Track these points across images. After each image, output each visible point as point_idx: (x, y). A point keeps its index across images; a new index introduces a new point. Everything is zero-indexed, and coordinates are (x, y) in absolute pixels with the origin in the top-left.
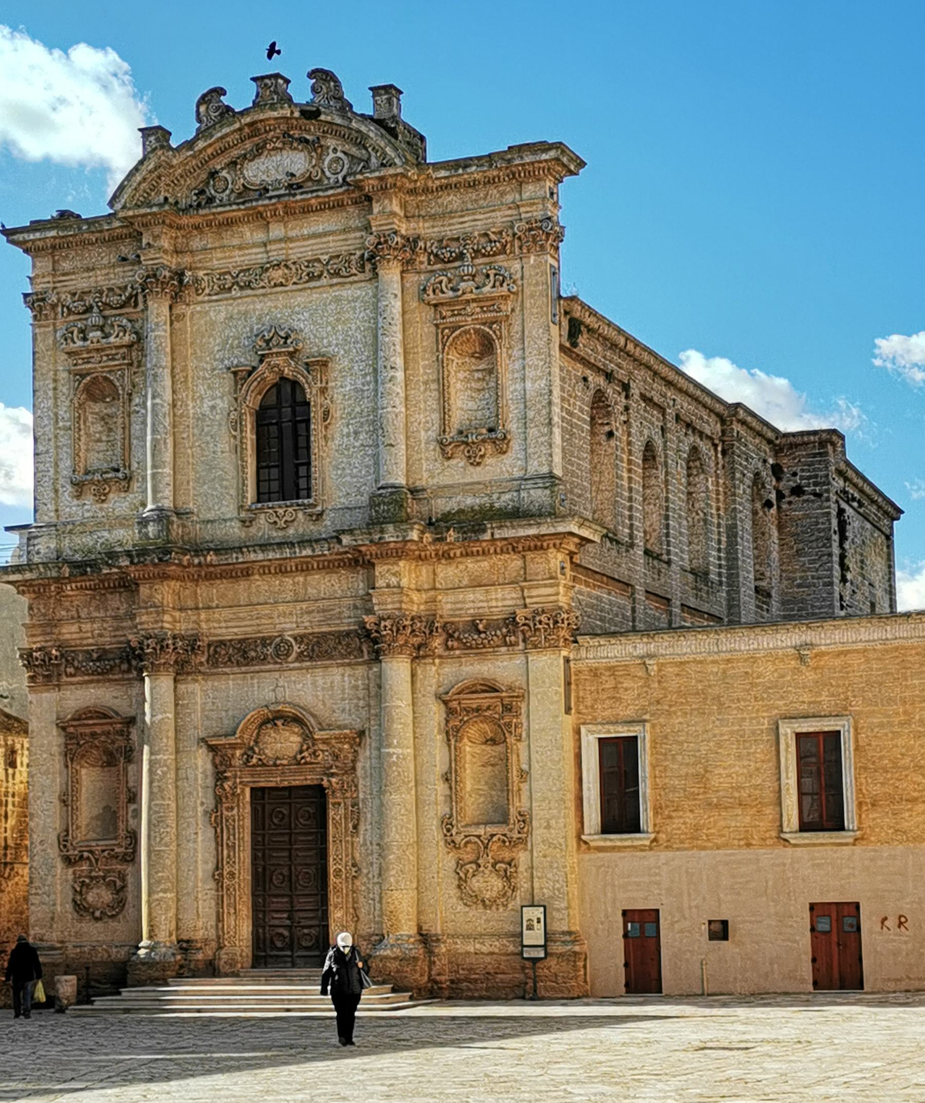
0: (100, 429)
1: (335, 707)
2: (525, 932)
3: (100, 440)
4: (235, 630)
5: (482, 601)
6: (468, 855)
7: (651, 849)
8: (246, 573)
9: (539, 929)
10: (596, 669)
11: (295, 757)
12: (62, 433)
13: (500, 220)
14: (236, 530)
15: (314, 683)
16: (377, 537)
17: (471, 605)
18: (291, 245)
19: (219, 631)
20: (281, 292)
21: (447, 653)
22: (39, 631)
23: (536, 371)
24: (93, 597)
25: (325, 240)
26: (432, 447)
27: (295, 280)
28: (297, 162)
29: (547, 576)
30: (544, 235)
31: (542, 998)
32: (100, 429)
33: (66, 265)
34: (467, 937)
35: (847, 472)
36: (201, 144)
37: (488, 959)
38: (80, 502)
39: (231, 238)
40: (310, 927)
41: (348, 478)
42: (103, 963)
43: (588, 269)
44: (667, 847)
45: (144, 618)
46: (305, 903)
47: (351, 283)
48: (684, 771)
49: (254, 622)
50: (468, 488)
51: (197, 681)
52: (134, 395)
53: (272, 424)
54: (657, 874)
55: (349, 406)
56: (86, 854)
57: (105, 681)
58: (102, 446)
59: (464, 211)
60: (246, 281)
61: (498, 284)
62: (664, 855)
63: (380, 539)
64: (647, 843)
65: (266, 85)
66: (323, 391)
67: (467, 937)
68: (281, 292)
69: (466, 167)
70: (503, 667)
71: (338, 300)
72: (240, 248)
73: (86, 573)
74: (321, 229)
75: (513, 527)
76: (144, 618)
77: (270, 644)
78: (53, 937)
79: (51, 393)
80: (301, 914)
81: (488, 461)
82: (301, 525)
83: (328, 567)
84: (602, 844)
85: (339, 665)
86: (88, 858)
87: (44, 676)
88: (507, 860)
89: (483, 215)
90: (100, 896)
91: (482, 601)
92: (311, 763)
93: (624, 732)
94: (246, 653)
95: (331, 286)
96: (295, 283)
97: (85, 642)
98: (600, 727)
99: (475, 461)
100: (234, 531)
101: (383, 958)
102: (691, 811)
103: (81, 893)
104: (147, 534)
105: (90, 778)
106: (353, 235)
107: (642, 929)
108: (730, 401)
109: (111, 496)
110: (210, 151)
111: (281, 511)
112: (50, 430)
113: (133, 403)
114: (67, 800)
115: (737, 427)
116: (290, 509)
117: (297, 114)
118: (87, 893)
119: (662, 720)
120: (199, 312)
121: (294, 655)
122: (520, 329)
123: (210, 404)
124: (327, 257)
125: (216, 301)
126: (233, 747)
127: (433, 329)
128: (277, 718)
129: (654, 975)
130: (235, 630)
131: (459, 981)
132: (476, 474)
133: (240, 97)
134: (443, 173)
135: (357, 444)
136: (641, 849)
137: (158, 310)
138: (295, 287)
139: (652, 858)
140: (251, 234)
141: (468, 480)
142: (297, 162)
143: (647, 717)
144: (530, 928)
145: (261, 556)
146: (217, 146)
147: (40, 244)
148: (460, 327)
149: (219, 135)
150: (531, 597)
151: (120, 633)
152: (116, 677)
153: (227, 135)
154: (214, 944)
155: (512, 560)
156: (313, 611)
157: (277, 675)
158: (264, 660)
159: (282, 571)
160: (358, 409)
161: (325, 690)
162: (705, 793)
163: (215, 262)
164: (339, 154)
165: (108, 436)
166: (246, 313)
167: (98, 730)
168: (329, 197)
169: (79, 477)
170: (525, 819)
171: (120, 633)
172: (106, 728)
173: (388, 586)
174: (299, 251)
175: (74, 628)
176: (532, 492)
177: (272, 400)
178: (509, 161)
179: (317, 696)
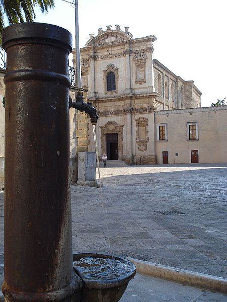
23: (151, 73)
30: (151, 50)
35: (195, 88)
43: (156, 55)
60: (106, 57)
66: (117, 74)
70: (146, 116)
82: (114, 94)
89: (144, 47)
100: (104, 95)
107: (165, 154)
108: (186, 80)
112: (8, 181)
115: (179, 80)
128: (111, 123)
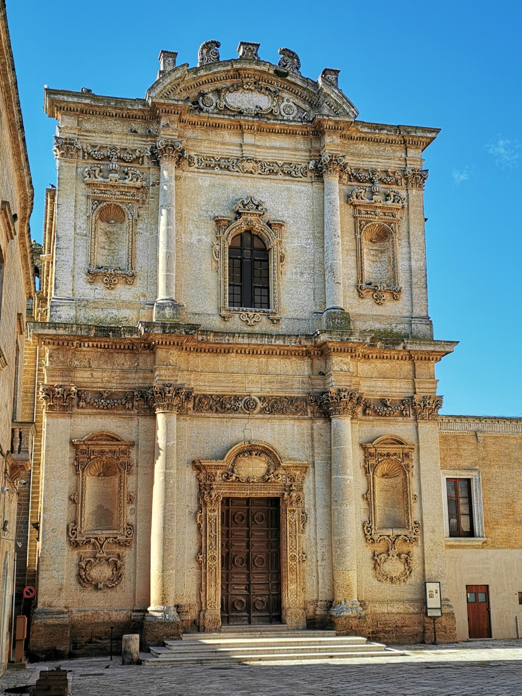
0: (104, 240)
1: (287, 446)
2: (428, 598)
3: (103, 248)
4: (216, 388)
5: (386, 388)
6: (380, 548)
7: (483, 548)
8: (227, 351)
9: (437, 596)
10: (446, 436)
11: (263, 477)
12: (79, 237)
13: (393, 165)
14: (217, 323)
15: (273, 429)
16: (346, 338)
17: (379, 389)
18: (258, 150)
19: (203, 388)
20: (250, 177)
21: (364, 418)
22: (58, 373)
24: (102, 353)
25: (281, 152)
26: (352, 290)
27: (260, 172)
28: (264, 102)
29: (429, 377)
31: (441, 643)
32: (104, 240)
33: (87, 126)
34: (382, 602)
36: (202, 73)
37: (397, 617)
38: (93, 286)
39: (214, 135)
40: (262, 595)
41: (296, 301)
42: (104, 623)
44: (492, 546)
45: (162, 372)
46: (259, 578)
47: (298, 181)
48: (500, 500)
49: (230, 385)
50: (377, 318)
51: (186, 420)
52: (139, 222)
53: (237, 259)
54: (487, 563)
55: (297, 256)
56: (93, 540)
57: (111, 414)
58: (105, 252)
59: (371, 156)
60: (225, 165)
61: (396, 201)
62: (491, 552)
63: (348, 339)
64: (480, 543)
65: (250, 49)
67: (382, 602)
68: (250, 177)
69: (382, 129)
71: (288, 189)
72: (223, 144)
73: (108, 336)
74: (278, 144)
75: (420, 344)
76: (162, 372)
77: (241, 400)
78: (60, 604)
79: (73, 208)
80: (256, 587)
81: (387, 303)
82: (263, 325)
83: (286, 354)
84: (453, 543)
85: (291, 419)
86: (94, 544)
87: (61, 406)
88: (405, 552)
89: (385, 159)
90: (102, 572)
91: (386, 388)
92: (274, 482)
93: (465, 475)
94: (223, 405)
95: (285, 180)
96: (259, 174)
97: (95, 385)
98: (452, 471)
99: (378, 301)
100: (216, 323)
101: (346, 618)
102: (505, 525)
103: (85, 570)
104: (164, 316)
105: (91, 483)
106: (300, 153)
109: (118, 286)
110: (204, 79)
111: (251, 314)
113: (138, 227)
114: (75, 500)
116: (258, 314)
117: (271, 72)
118: (91, 569)
119: (486, 470)
120: (189, 177)
121: (258, 409)
122: (406, 230)
123: (198, 237)
124: (282, 163)
125: (204, 173)
126: (217, 467)
127: (352, 220)
128: (251, 450)
129: (486, 626)
130: (216, 388)
131: (378, 632)
132: (379, 310)
133: (231, 51)
134: (366, 130)
135: (302, 280)
136: (474, 547)
137: (168, 170)
138: (259, 176)
139: (483, 553)
140: (230, 137)
141: (375, 313)
142: (264, 102)
143: (477, 467)
144: (431, 596)
145: (246, 341)
146: (212, 77)
147: (72, 106)
148: (371, 222)
149: (216, 70)
150: (419, 388)
151: (125, 381)
152: (120, 412)
153: (218, 72)
154: (197, 609)
155: (405, 365)
156: (273, 382)
157: (246, 421)
158: (236, 410)
159: (253, 353)
160: (302, 259)
161: (287, 435)
162: (513, 515)
163: (203, 149)
164: (291, 104)
165: (109, 246)
166: (224, 185)
167: (106, 449)
168: (289, 126)
169: (93, 269)
170: (419, 525)
171: (125, 381)
172: (113, 448)
173: (342, 370)
174: (261, 155)
175: (87, 374)
176: (419, 325)
177: (238, 244)
178: (408, 132)
179: (274, 438)
